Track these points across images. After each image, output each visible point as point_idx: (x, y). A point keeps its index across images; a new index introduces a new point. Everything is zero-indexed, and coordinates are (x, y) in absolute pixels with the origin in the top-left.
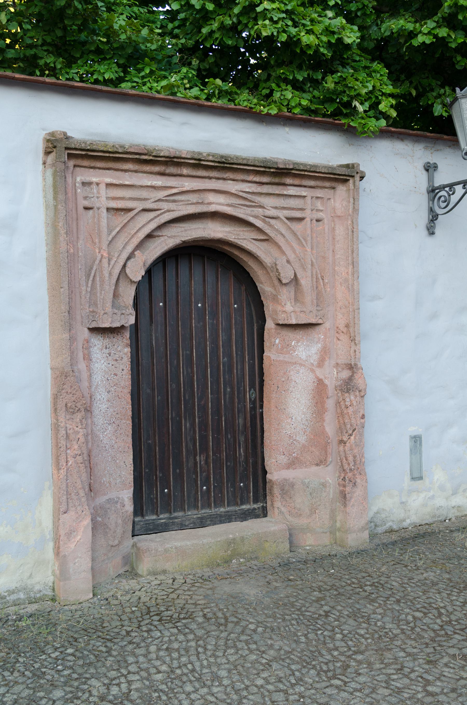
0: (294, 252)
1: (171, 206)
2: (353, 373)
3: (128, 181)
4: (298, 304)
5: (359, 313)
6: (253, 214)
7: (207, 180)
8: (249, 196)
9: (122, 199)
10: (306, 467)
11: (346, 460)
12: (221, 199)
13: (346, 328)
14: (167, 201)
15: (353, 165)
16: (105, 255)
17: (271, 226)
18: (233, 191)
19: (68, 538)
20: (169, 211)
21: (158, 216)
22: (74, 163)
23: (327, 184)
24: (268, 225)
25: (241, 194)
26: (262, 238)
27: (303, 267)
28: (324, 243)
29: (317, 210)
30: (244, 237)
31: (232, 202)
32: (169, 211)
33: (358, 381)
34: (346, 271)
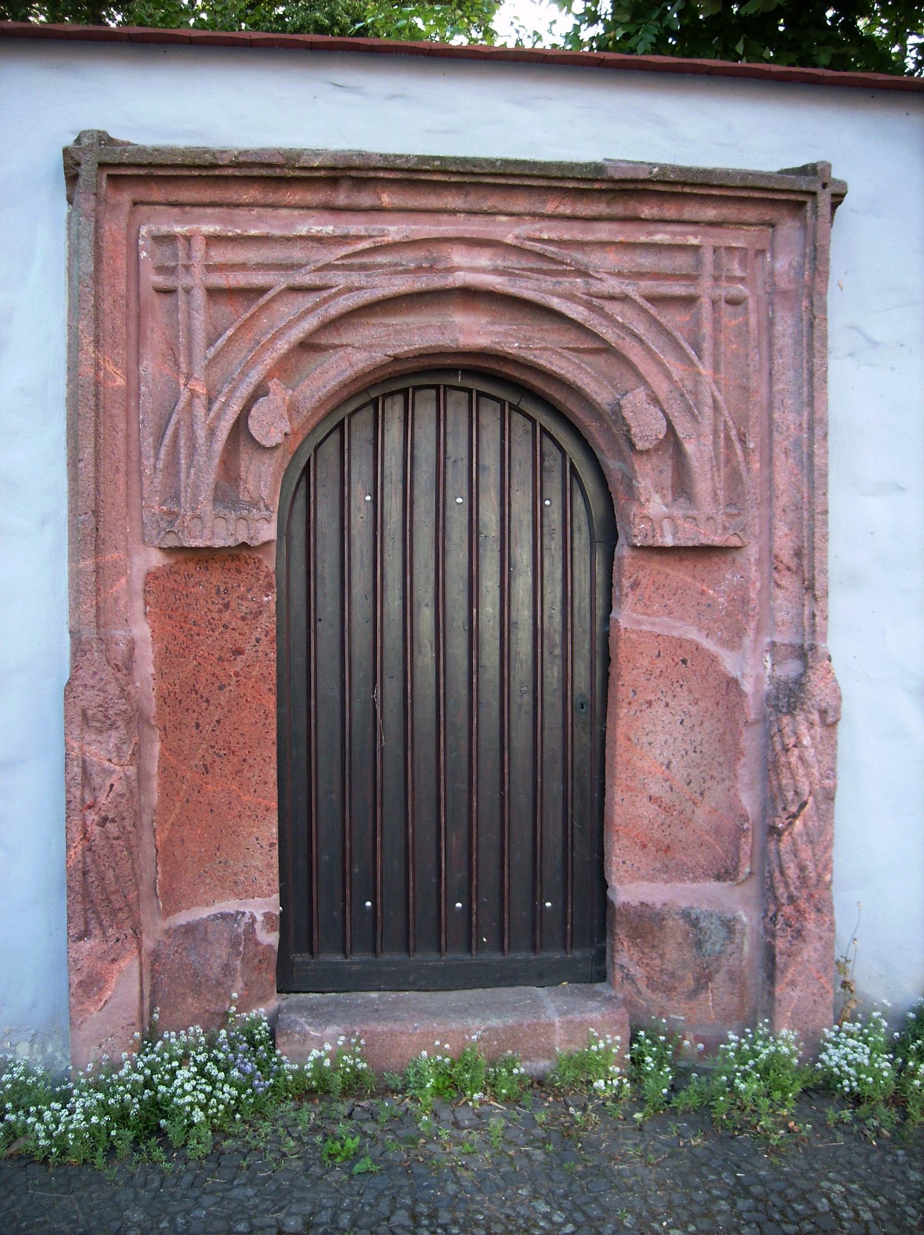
0: (668, 376)
1: (356, 278)
2: (806, 666)
3: (256, 227)
4: (682, 500)
5: (825, 523)
6: (559, 289)
7: (445, 217)
8: (551, 249)
9: (243, 267)
10: (695, 879)
11: (782, 873)
12: (484, 259)
13: (795, 560)
14: (344, 267)
15: (814, 166)
16: (201, 390)
17: (609, 318)
18: (509, 239)
19: (84, 992)
20: (350, 289)
21: (325, 301)
22: (133, 196)
23: (751, 214)
24: (600, 316)
25: (528, 245)
26: (595, 346)
27: (692, 413)
28: (747, 355)
29: (731, 279)
30: (544, 344)
31: (508, 263)
32: (350, 289)
33: (817, 689)
34: (798, 423)
